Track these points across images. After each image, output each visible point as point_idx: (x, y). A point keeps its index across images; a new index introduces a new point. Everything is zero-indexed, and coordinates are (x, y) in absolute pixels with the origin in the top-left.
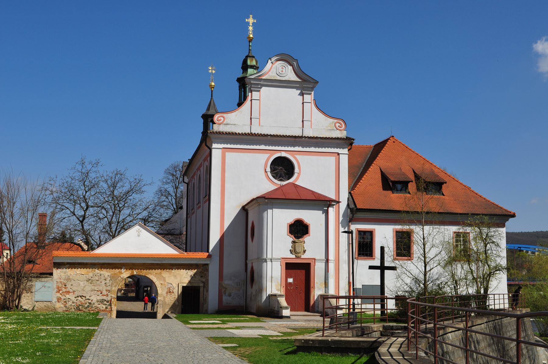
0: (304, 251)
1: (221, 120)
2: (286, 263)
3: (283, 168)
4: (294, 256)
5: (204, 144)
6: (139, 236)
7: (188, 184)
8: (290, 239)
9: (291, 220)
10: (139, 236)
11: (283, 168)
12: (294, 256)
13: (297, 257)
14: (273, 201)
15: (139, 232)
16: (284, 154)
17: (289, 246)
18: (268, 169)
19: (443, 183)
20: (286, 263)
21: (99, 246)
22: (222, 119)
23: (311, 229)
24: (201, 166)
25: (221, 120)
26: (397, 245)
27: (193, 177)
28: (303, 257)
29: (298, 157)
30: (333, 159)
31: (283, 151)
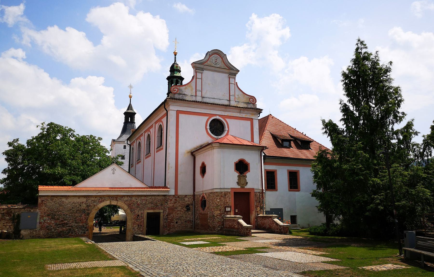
0: (247, 183)
1: (175, 90)
2: (234, 192)
3: (217, 127)
4: (239, 187)
5: (163, 105)
6: (113, 173)
7: (130, 145)
8: (237, 174)
9: (236, 160)
10: (113, 173)
11: (217, 127)
12: (239, 187)
13: (243, 188)
14: (223, 145)
15: (114, 170)
16: (218, 117)
17: (236, 179)
18: (208, 127)
19: (311, 142)
20: (234, 192)
21: (84, 177)
22: (177, 90)
23: (251, 167)
24: (152, 126)
25: (175, 90)
26: (274, 183)
27: (134, 142)
28: (245, 187)
29: (227, 120)
30: (249, 123)
31: (218, 114)
